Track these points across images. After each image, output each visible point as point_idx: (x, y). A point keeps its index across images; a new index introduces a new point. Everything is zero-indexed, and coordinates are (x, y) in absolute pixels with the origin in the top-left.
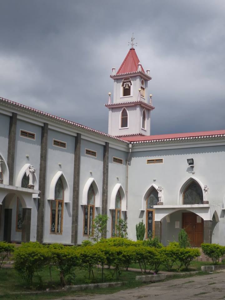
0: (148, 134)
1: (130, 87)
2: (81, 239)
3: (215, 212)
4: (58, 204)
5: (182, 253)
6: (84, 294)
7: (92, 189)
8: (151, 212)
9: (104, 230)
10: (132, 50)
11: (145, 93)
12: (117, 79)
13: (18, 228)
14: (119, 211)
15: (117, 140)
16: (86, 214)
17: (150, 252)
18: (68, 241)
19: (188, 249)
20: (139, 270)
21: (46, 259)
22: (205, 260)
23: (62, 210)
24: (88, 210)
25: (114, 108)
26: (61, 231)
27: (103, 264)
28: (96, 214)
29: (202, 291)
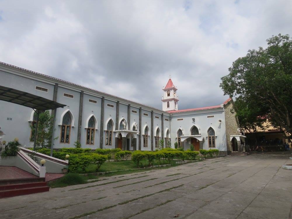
0: (177, 110)
1: (170, 93)
2: (155, 149)
3: (204, 138)
4: (146, 136)
5: (192, 153)
6: (158, 169)
7: (158, 130)
8: (180, 138)
9: (163, 145)
10: (170, 79)
11: (175, 95)
12: (165, 90)
13: (132, 146)
14: (168, 138)
15: (166, 112)
16: (156, 139)
17: (180, 153)
18: (150, 150)
19: (194, 152)
20: (177, 160)
21: (144, 156)
22: (200, 156)
23: (147, 138)
24: (157, 138)
25: (164, 101)
26: (147, 146)
27: (164, 158)
28: (160, 140)
29: (202, 167)
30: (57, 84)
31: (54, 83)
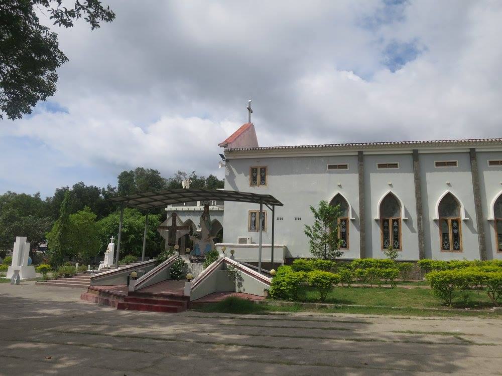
30: (360, 153)
31: (467, 149)
